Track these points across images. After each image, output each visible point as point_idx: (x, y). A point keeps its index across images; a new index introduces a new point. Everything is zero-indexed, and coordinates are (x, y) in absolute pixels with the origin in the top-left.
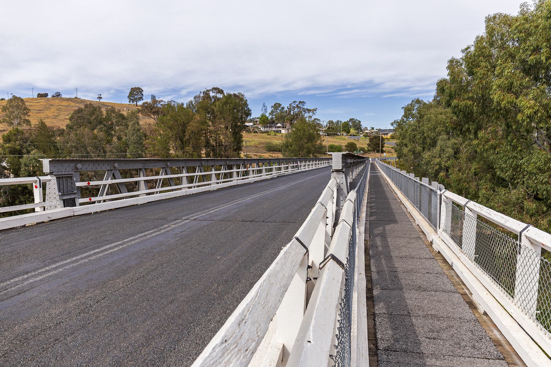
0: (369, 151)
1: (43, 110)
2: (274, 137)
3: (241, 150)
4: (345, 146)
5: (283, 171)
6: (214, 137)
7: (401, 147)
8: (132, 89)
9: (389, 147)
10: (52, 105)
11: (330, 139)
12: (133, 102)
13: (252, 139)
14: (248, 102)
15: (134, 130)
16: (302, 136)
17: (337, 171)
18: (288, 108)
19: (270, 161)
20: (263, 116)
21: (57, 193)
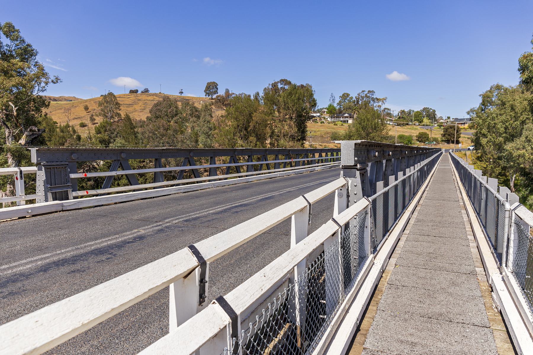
1: (132, 104)
2: (340, 127)
3: (305, 140)
4: (416, 136)
9: (465, 138)
10: (139, 100)
11: (400, 129)
13: (318, 129)
18: (356, 97)
20: (330, 106)
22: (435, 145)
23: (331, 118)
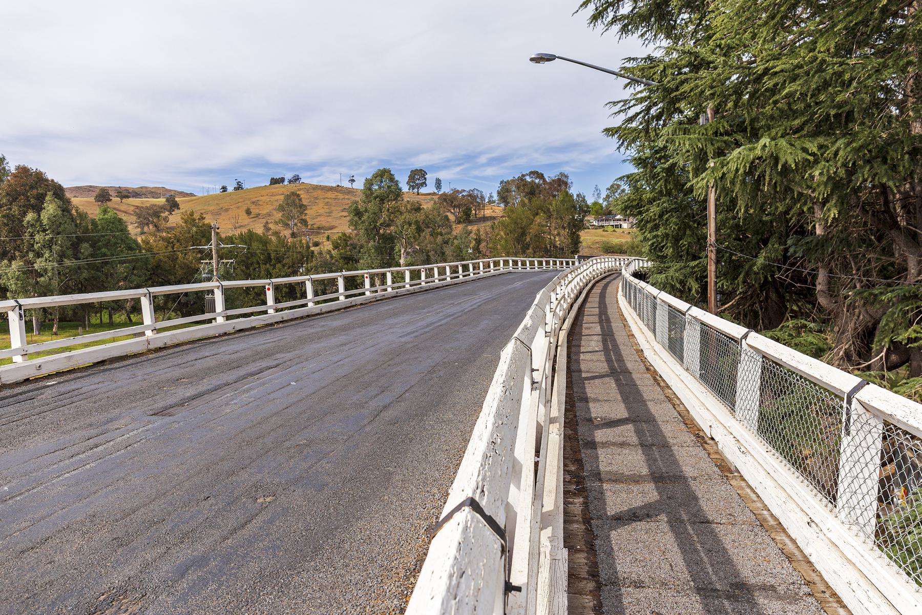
2: (612, 235)
12: (413, 189)
15: (466, 233)
23: (598, 221)
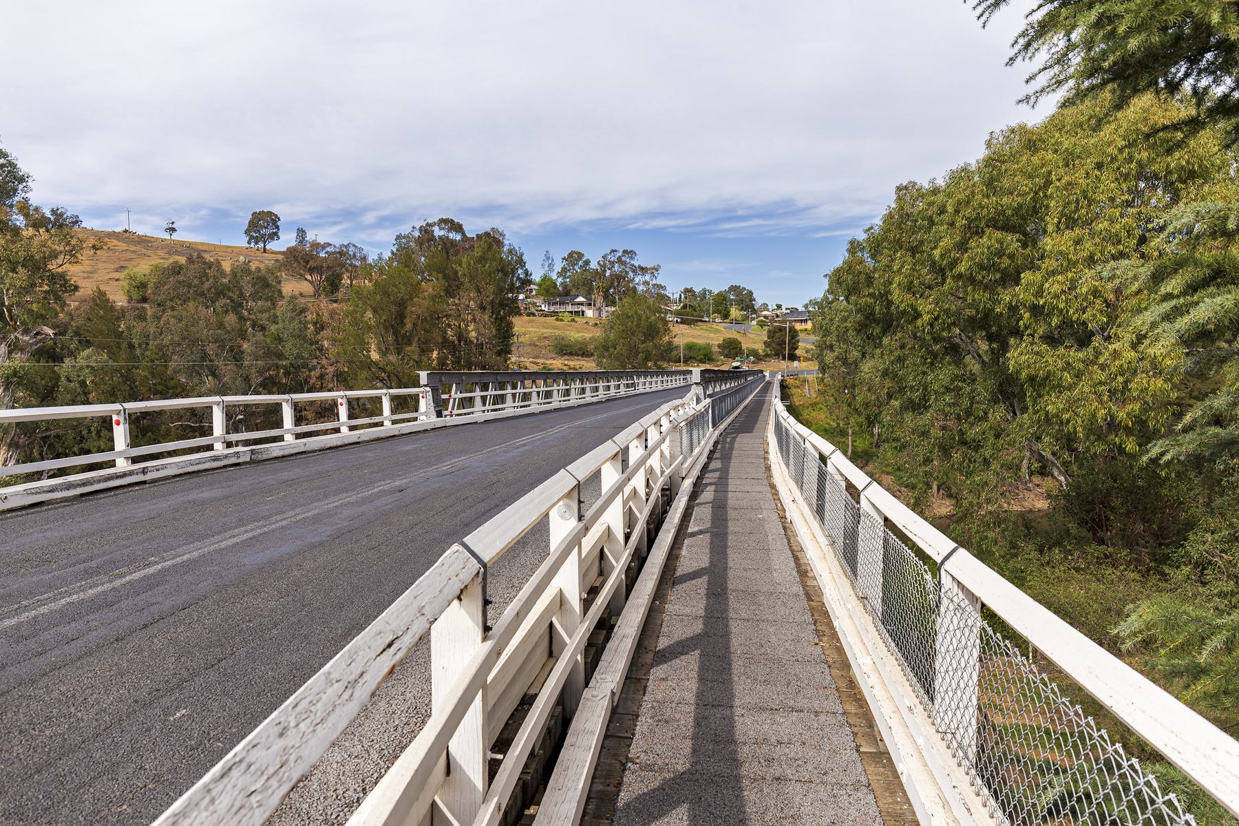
0: (767, 355)
2: (569, 326)
4: (719, 346)
5: (612, 392)
6: (454, 324)
7: (822, 350)
8: (254, 214)
11: (687, 331)
12: (256, 243)
14: (524, 258)
15: (293, 310)
16: (634, 328)
17: (696, 384)
19: (567, 376)
21: (432, 404)
22: (753, 363)
23: (549, 304)
